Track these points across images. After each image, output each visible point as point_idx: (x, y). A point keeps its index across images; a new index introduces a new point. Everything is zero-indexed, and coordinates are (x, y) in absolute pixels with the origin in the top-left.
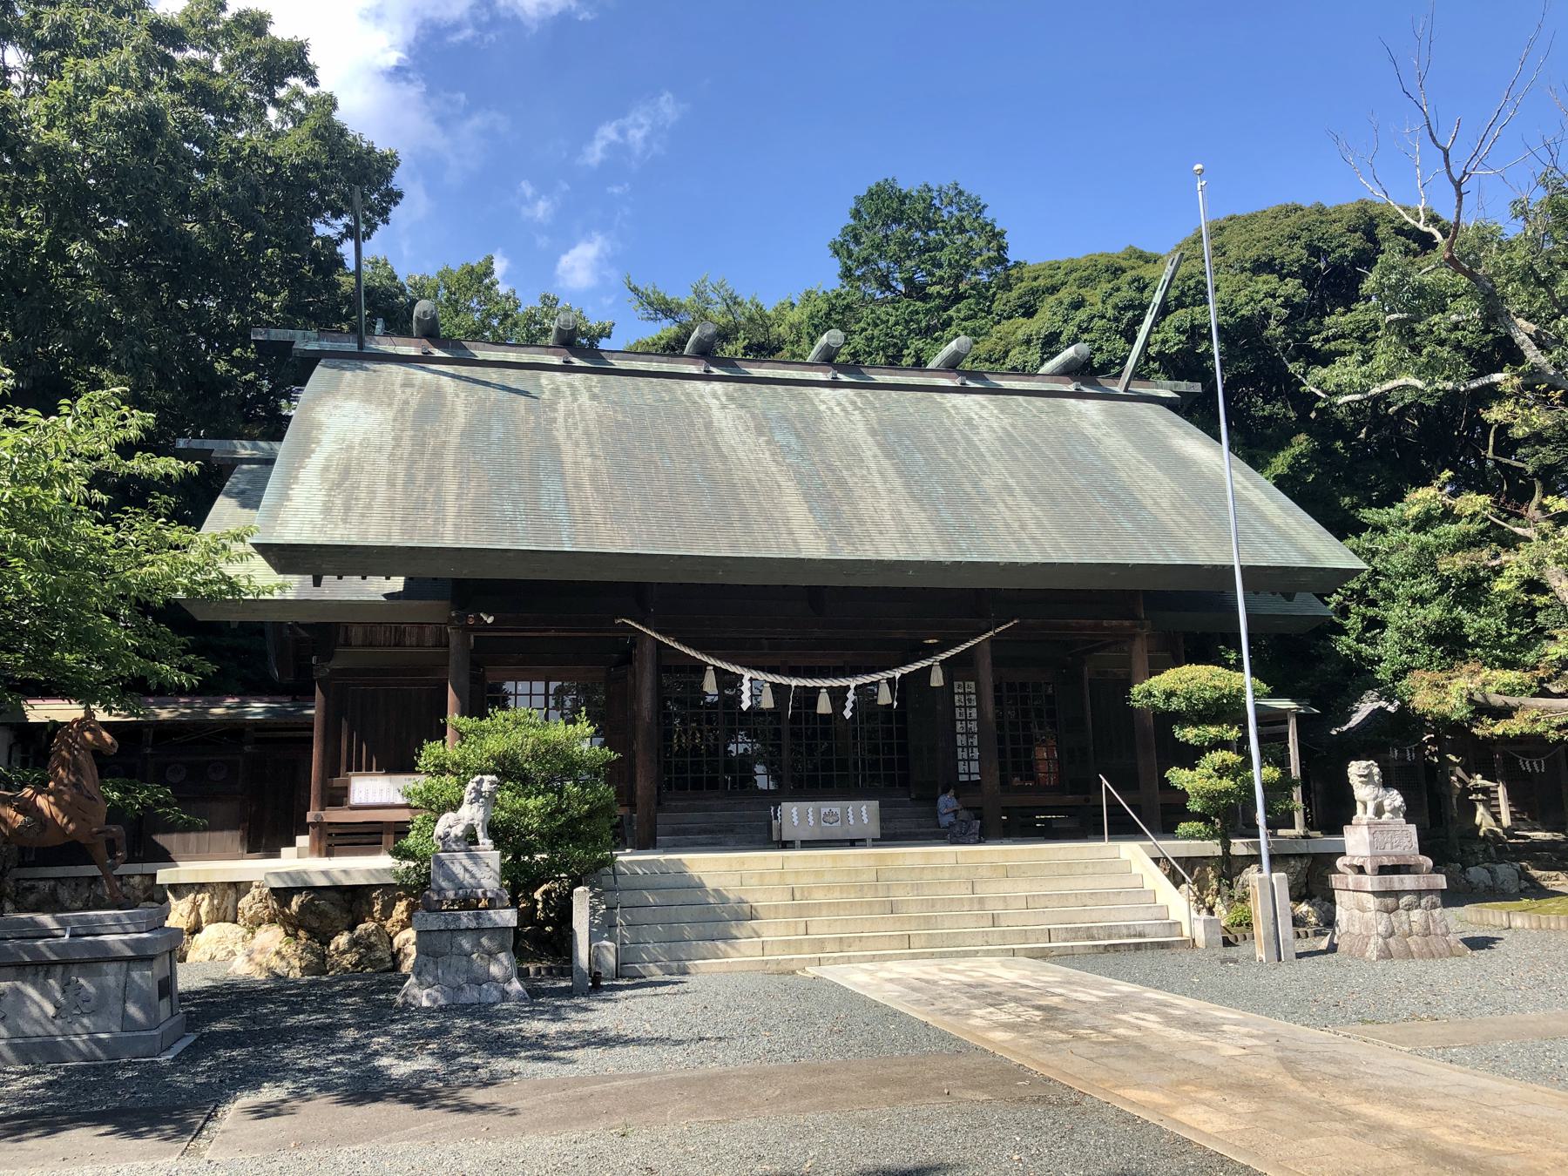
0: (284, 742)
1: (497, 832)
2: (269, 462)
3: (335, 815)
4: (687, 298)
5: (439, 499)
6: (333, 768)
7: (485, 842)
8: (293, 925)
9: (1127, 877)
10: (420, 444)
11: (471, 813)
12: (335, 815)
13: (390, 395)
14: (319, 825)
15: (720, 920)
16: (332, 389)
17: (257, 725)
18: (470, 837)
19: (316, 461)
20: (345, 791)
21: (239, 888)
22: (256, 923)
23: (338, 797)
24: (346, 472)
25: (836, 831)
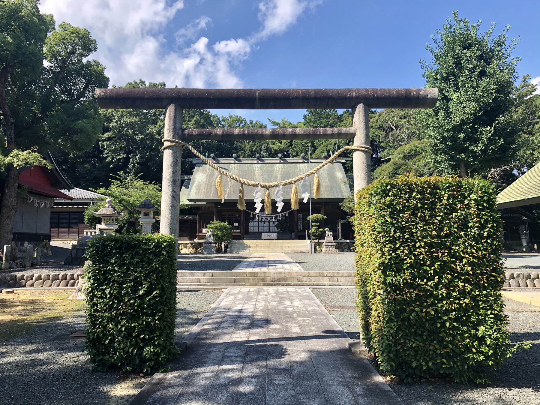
0: (194, 222)
1: (213, 235)
2: (190, 179)
3: (200, 234)
4: (280, 121)
5: (211, 191)
6: (200, 227)
7: (212, 237)
8: (193, 247)
9: (306, 244)
10: (209, 181)
11: (210, 233)
12: (200, 234)
13: (206, 171)
14: (198, 236)
15: (245, 247)
16: (198, 171)
17: (191, 220)
18: (210, 236)
19: (195, 185)
20: (202, 231)
21: (187, 244)
22: (189, 248)
23: (201, 232)
24: (199, 187)
25: (270, 238)
